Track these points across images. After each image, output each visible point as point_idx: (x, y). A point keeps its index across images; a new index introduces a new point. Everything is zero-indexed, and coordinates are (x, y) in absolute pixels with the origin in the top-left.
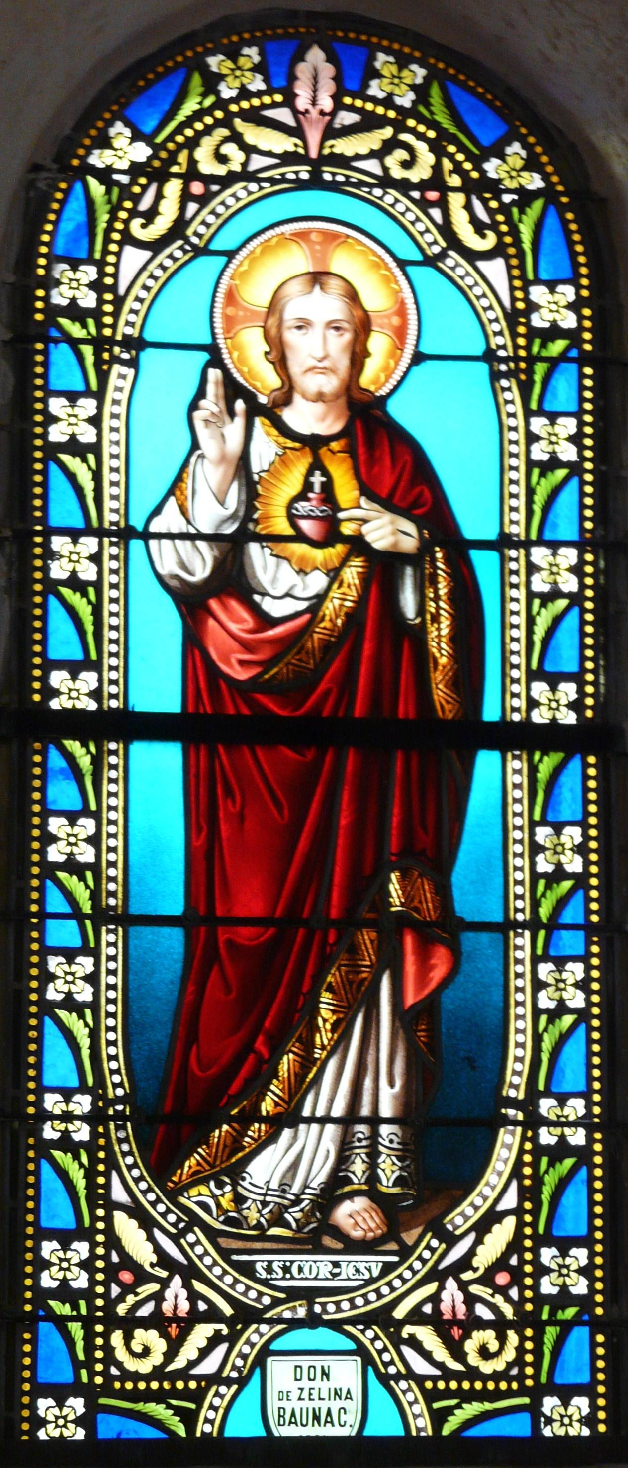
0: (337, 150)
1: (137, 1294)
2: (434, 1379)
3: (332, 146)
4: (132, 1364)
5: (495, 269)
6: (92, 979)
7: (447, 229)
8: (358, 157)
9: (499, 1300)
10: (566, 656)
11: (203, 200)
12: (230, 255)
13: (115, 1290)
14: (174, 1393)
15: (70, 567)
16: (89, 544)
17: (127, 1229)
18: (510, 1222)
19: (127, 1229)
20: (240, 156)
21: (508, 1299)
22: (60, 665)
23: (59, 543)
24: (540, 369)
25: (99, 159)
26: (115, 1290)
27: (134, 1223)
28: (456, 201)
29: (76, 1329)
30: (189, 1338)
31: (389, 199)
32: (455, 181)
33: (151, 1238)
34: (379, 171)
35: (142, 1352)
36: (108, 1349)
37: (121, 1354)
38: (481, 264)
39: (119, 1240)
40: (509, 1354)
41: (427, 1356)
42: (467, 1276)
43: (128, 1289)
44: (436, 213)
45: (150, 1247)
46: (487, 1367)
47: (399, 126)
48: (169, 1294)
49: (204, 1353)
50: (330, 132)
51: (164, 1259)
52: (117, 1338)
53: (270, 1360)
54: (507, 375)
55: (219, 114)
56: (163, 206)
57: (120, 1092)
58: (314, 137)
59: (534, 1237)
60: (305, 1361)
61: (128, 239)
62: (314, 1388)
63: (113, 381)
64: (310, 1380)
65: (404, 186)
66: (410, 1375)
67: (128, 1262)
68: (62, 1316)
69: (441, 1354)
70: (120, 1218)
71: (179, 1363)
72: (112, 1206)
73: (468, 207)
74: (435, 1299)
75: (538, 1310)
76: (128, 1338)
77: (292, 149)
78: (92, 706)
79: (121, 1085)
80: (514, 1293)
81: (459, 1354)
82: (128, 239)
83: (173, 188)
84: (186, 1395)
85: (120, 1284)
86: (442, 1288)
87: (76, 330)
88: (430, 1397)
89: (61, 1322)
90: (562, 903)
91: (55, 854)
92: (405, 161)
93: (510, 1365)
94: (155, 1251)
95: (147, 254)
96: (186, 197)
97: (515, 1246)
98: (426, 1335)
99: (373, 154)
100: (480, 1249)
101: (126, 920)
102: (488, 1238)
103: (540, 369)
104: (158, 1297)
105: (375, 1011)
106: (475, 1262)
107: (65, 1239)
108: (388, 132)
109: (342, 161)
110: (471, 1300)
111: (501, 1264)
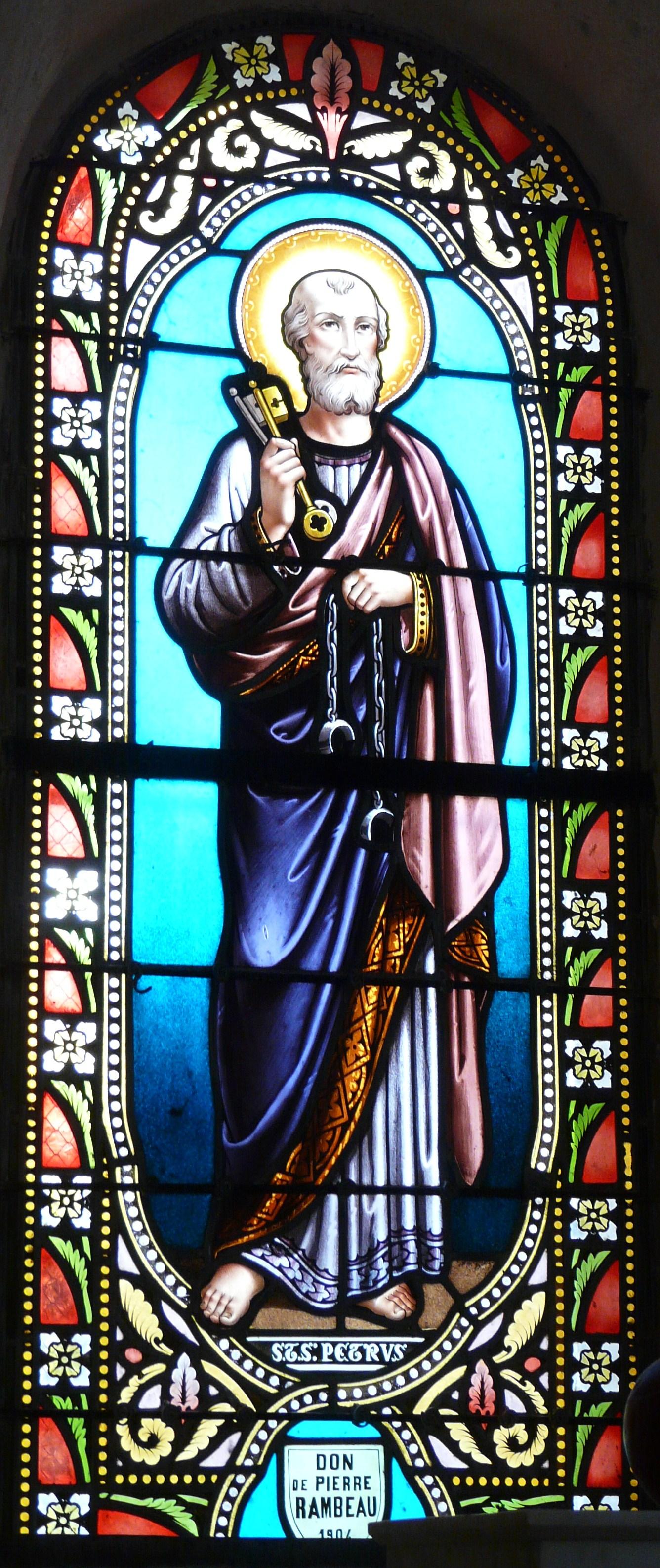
0: (356, 152)
1: (141, 1376)
2: (462, 1473)
3: (352, 147)
4: (138, 1455)
5: (519, 288)
6: (94, 1048)
7: (469, 244)
8: (378, 161)
9: (529, 1388)
10: (594, 701)
11: (218, 194)
12: (246, 256)
13: (120, 1372)
14: (182, 1488)
15: (65, 1058)
16: (93, 556)
17: (133, 1300)
18: (540, 1298)
19: (133, 1300)
20: (253, 149)
21: (539, 1387)
22: (63, 394)
23: (61, 554)
24: (564, 394)
25: (105, 141)
26: (120, 1372)
27: (140, 1294)
28: (478, 215)
29: (78, 1425)
30: (195, 1435)
31: (411, 208)
32: (476, 194)
33: (157, 1311)
34: (397, 177)
35: (149, 1444)
36: (113, 1438)
37: (127, 1443)
38: (504, 282)
39: (125, 1314)
40: (539, 1447)
41: (453, 1446)
42: (499, 1359)
43: (134, 1369)
44: (458, 227)
45: (155, 1320)
46: (514, 1461)
47: (420, 134)
48: (176, 1375)
49: (215, 1443)
50: (348, 133)
51: (170, 1335)
52: (122, 1429)
53: (287, 1448)
54: (533, 399)
55: (234, 105)
56: (174, 200)
57: (124, 1152)
58: (332, 124)
59: (566, 1326)
60: (327, 1450)
61: (135, 231)
62: (334, 1484)
63: (119, 381)
64: (332, 1468)
65: (424, 196)
66: (435, 1468)
67: (133, 1338)
68: (62, 1411)
69: (467, 1444)
70: (125, 1286)
71: (188, 1454)
72: (117, 1275)
73: (492, 222)
74: (463, 1384)
75: (570, 1405)
76: (134, 1429)
77: (309, 147)
78: (95, 737)
79: (125, 1144)
80: (544, 1379)
81: (487, 1447)
82: (135, 231)
83: (184, 186)
84: (194, 1489)
85: (126, 1363)
86: (471, 1371)
87: (78, 323)
88: (457, 1494)
89: (60, 1418)
90: (590, 973)
91: (53, 1062)
92: (424, 169)
93: (538, 1459)
94: (160, 1326)
95: (157, 248)
96: (199, 190)
97: (545, 1327)
98: (458, 1431)
99: (392, 159)
100: (511, 1328)
101: (132, 969)
102: (517, 1315)
103: (564, 394)
104: (164, 1380)
105: (409, 1000)
106: (507, 1341)
107: (71, 1019)
108: (407, 135)
109: (362, 164)
110: (501, 1385)
111: (530, 1348)
